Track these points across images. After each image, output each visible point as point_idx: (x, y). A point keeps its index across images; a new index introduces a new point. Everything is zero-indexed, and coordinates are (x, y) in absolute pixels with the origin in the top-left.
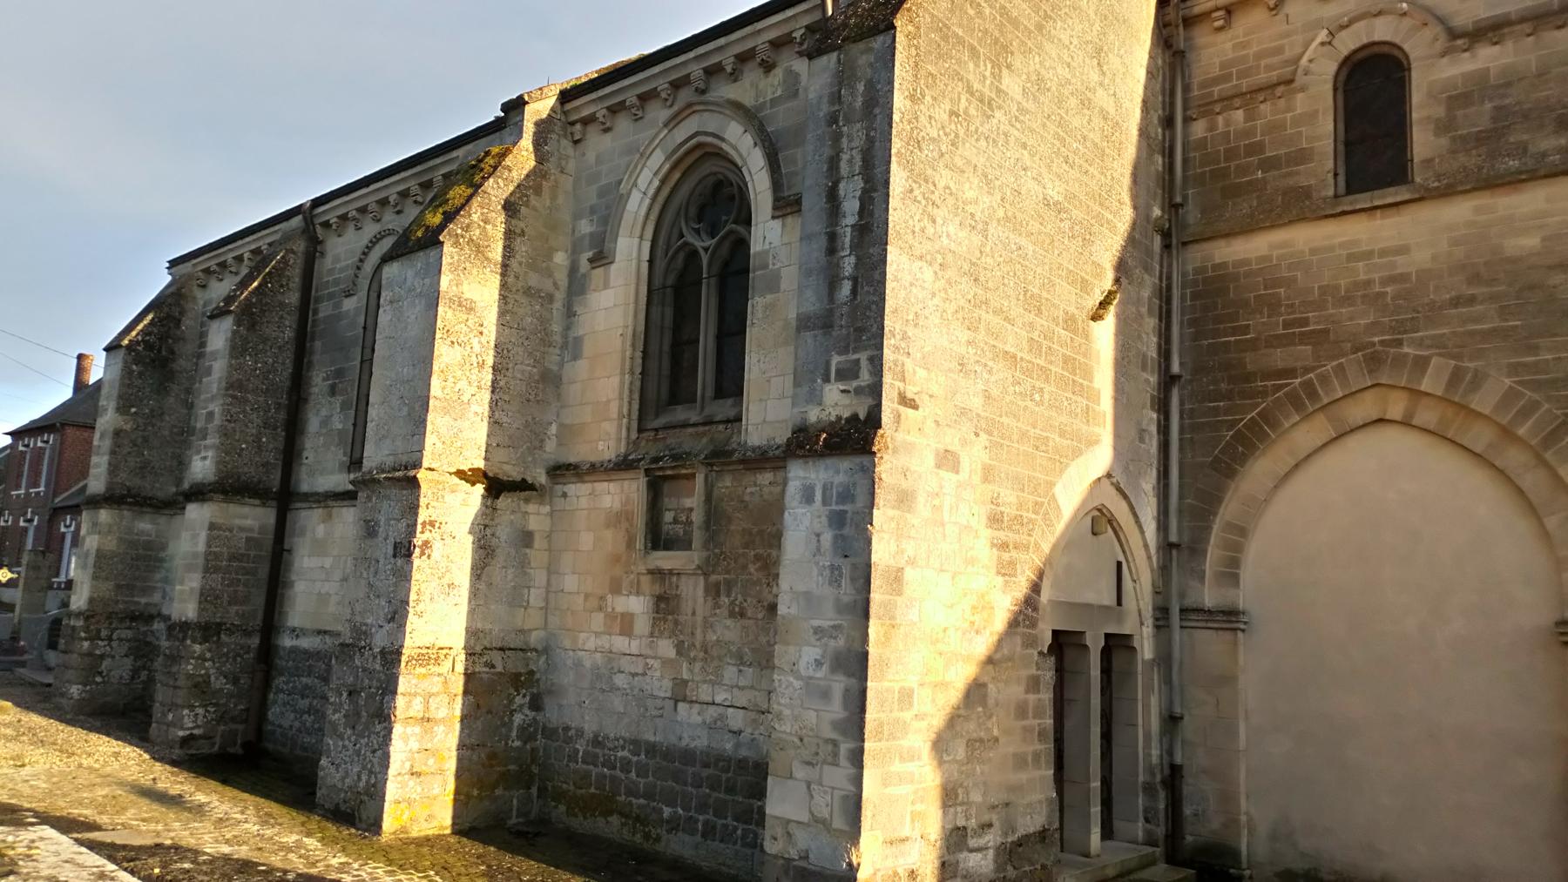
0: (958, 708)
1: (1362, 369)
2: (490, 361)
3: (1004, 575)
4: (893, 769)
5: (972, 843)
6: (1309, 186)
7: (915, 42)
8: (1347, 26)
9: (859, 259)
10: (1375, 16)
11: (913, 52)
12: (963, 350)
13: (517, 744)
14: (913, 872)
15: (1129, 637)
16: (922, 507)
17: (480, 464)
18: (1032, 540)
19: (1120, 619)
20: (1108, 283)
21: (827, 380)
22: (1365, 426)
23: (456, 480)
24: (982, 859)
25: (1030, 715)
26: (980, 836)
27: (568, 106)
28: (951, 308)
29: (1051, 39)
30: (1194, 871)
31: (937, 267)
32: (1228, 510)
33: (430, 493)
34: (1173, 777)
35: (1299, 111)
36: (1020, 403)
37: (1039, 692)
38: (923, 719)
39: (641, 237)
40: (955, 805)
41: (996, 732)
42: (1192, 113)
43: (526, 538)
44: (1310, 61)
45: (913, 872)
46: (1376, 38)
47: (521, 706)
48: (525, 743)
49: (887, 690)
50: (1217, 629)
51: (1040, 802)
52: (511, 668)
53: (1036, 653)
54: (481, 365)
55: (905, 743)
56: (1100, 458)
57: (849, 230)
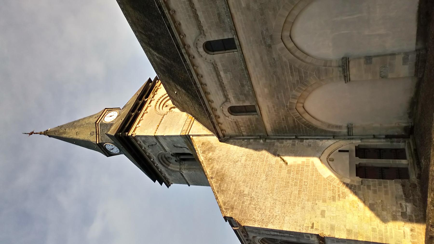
0: (375, 213)
3: (345, 197)
4: (389, 235)
5: (405, 210)
6: (256, 118)
7: (245, 220)
8: (225, 115)
9: (286, 233)
10: (223, 111)
11: (247, 221)
12: (300, 208)
14: (411, 230)
15: (356, 147)
16: (333, 223)
18: (337, 186)
19: (352, 151)
20: (279, 159)
21: (310, 239)
22: (304, 109)
24: (408, 207)
25: (376, 188)
26: (403, 207)
28: (292, 212)
29: (235, 178)
30: (411, 136)
31: (285, 215)
32: (325, 128)
34: (388, 137)
35: (241, 120)
36: (308, 189)
37: (370, 185)
38: (378, 225)
40: (396, 216)
41: (380, 201)
42: (242, 135)
44: (231, 119)
45: (411, 230)
46: (227, 111)
49: (372, 236)
50: (352, 130)
51: (395, 186)
53: (362, 186)
55: (383, 231)
56: (315, 160)
57: (280, 234)
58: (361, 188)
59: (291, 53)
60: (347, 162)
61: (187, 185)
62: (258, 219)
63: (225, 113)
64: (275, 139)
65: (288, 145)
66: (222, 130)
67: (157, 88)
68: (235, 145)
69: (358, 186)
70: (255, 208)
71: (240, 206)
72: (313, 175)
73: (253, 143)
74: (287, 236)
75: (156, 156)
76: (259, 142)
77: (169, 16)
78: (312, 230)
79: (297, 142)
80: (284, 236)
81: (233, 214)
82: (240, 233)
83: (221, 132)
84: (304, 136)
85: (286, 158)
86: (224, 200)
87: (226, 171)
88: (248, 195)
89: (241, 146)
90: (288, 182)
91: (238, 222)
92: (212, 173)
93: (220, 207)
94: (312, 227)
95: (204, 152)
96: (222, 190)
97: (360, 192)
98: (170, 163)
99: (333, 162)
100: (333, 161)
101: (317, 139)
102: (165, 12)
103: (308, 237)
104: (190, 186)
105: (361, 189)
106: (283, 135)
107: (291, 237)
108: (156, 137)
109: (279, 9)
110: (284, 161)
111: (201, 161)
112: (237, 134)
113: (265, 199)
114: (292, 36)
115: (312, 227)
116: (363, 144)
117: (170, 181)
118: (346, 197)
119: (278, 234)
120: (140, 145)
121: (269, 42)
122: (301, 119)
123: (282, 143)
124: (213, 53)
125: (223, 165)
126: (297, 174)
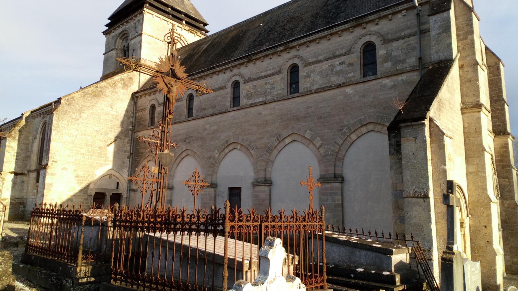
1: (412, 125)
2: (16, 155)
13: (20, 213)
15: (121, 194)
17: (13, 171)
20: (113, 140)
23: (8, 173)
27: (33, 114)
29: (96, 106)
33: (410, 154)
39: (40, 135)
42: (137, 112)
43: (23, 182)
47: (21, 207)
48: (22, 213)
52: (19, 201)
53: (87, 195)
54: (14, 156)
56: (109, 166)
58: (85, 195)
59: (180, 154)
60: (108, 187)
61: (104, 52)
62: (60, 124)
63: (152, 101)
64: (131, 138)
65: (126, 147)
66: (141, 96)
67: (195, 33)
68: (128, 106)
69: (87, 193)
70: (69, 122)
71: (70, 111)
72: (97, 163)
73: (129, 121)
74: (47, 144)
75: (128, 28)
76: (130, 125)
77: (209, 73)
78: (52, 161)
79: (128, 154)
80: (47, 142)
81: (63, 105)
82: (47, 109)
83: (139, 95)
84: (132, 159)
85: (113, 146)
86: (76, 97)
87: (103, 99)
88: (80, 117)
89: (127, 111)
90: (91, 146)
91: (57, 108)
92: (101, 87)
93: (69, 95)
94: (53, 161)
95: (122, 79)
96: (85, 96)
97: (82, 194)
98: (123, 40)
99: (108, 178)
100: (110, 178)
101: (129, 168)
102: (211, 71)
103: (46, 158)
104: (103, 55)
105: (84, 194)
106: (134, 144)
107: (47, 147)
108: (141, 34)
109: (201, 149)
110: (110, 144)
111: (114, 77)
112: (138, 108)
113: (77, 129)
114: (188, 156)
115: (53, 161)
116: (123, 198)
117: (108, 36)
118: (78, 185)
119: (48, 138)
120: (136, 16)
121: (187, 141)
122: (143, 158)
123: (127, 143)
124: (188, 99)
125: (108, 96)
126: (99, 153)
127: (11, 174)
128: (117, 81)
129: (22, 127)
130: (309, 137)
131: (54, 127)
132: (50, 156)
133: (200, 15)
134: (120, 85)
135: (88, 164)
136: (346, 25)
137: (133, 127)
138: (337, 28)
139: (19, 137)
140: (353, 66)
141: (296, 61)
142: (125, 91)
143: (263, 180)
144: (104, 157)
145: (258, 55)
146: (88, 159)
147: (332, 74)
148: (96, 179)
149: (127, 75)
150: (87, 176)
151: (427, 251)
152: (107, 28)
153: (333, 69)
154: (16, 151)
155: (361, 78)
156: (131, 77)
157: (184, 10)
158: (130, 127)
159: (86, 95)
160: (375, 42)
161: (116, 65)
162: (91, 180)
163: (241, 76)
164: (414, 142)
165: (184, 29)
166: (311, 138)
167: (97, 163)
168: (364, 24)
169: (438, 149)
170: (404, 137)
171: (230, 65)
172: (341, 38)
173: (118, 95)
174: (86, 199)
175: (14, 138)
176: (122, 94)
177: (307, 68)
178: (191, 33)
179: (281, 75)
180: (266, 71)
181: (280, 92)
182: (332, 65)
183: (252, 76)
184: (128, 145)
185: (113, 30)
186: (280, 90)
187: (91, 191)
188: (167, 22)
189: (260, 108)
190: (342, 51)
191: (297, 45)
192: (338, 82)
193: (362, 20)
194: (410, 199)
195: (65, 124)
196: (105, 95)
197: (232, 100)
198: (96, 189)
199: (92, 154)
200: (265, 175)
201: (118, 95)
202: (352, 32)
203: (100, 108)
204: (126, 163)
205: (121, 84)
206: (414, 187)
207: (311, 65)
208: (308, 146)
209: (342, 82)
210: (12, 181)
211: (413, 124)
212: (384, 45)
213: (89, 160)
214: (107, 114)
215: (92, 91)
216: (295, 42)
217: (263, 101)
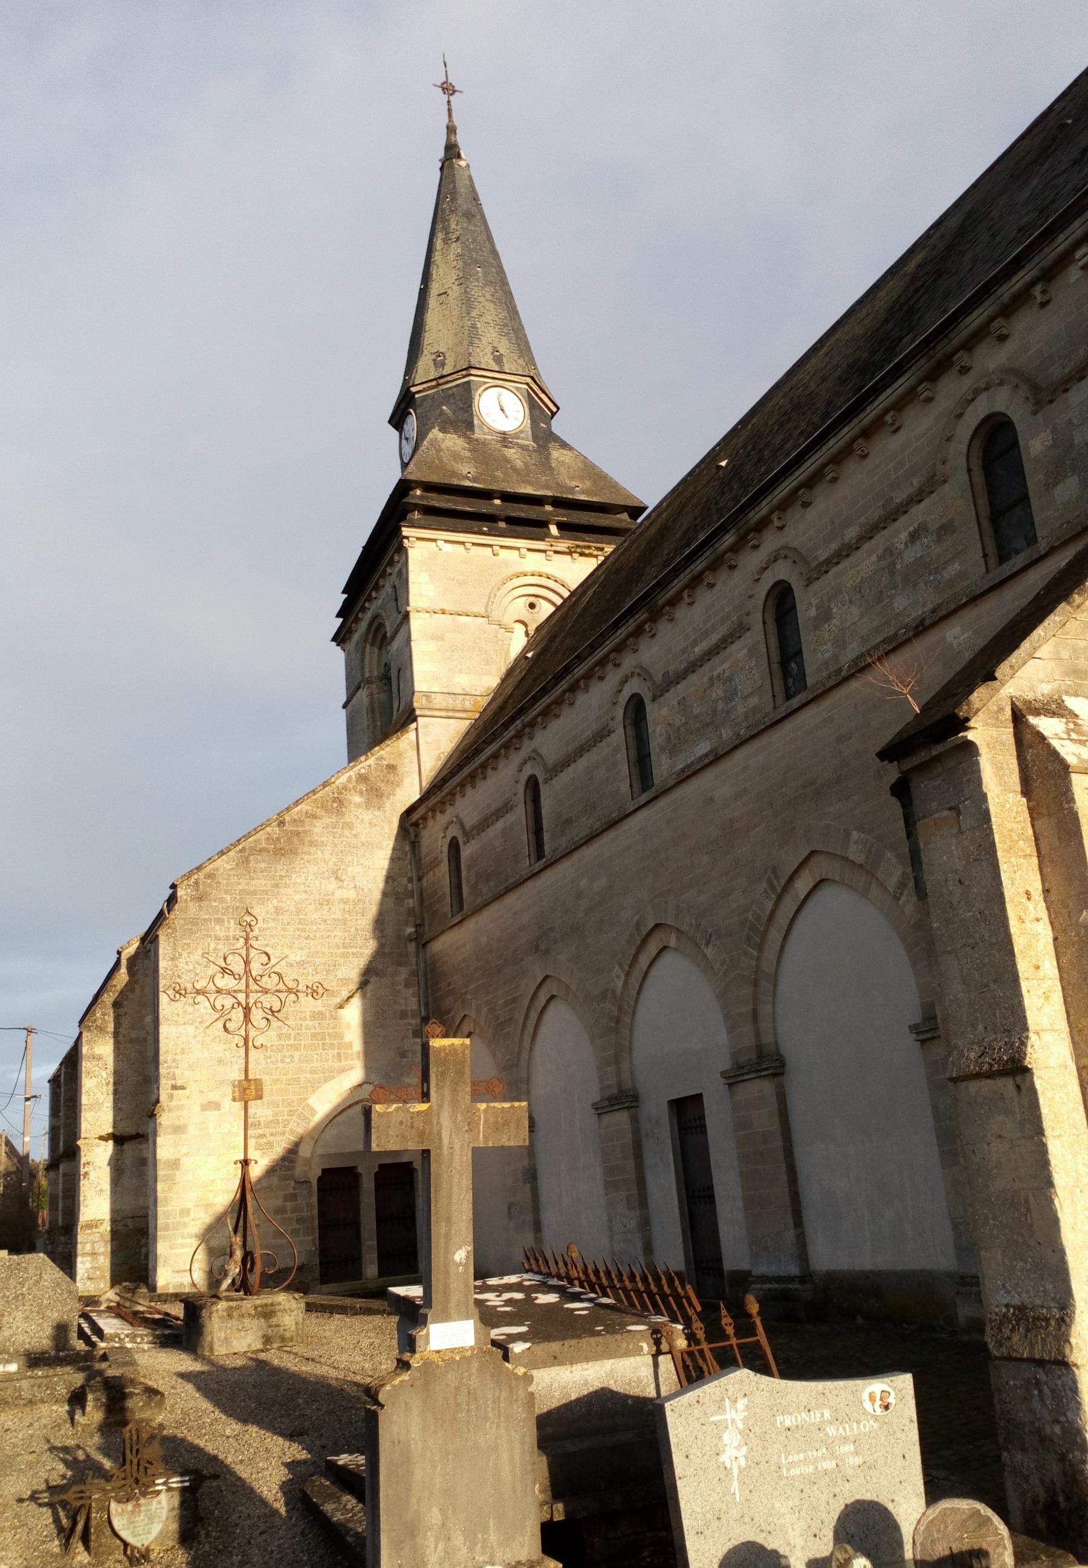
1: (937, 759)
17: (110, 1130)
20: (353, 986)
23: (97, 1141)
29: (286, 886)
53: (292, 1183)
54: (107, 1084)
61: (344, 699)
62: (181, 965)
66: (424, 818)
67: (595, 553)
69: (293, 1175)
71: (207, 917)
72: (313, 1072)
76: (406, 924)
78: (169, 1087)
86: (222, 870)
87: (306, 857)
89: (390, 878)
92: (295, 821)
93: (199, 868)
94: (174, 1087)
96: (248, 861)
97: (275, 1180)
106: (429, 984)
115: (174, 1087)
123: (407, 985)
125: (323, 844)
126: (314, 1036)
127: (103, 1143)
128: (345, 788)
129: (121, 992)
130: (860, 859)
131: (164, 978)
132: (163, 1071)
133: (614, 486)
134: (357, 799)
135: (284, 1078)
136: (901, 381)
137: (417, 926)
138: (877, 403)
139: (115, 1024)
140: (954, 532)
141: (782, 571)
142: (376, 813)
143: (754, 1056)
144: (332, 1044)
145: (670, 586)
146: (282, 1061)
147: (895, 587)
148: (318, 1124)
149: (377, 759)
150: (286, 1117)
151: (1053, 1323)
152: (341, 620)
153: (893, 564)
154: (112, 1069)
155: (988, 571)
156: (392, 762)
157: (548, 487)
158: (410, 930)
159: (252, 858)
160: (1009, 413)
161: (373, 734)
162: (300, 1130)
163: (643, 673)
164: (955, 831)
165: (556, 552)
166: (867, 858)
167: (313, 1072)
168: (958, 355)
169: (1059, 839)
170: (924, 817)
171: (608, 645)
172: (901, 437)
173: (354, 832)
174: (293, 1197)
175: (102, 1029)
176: (367, 826)
177: (816, 586)
178: (582, 558)
179: (748, 639)
180: (706, 634)
181: (753, 701)
182: (889, 551)
183: (672, 667)
184: (411, 990)
185: (353, 625)
186: (752, 693)
187: (307, 1168)
188: (489, 549)
189: (707, 780)
190: (912, 484)
191: (772, 512)
192: (916, 613)
193: (946, 341)
194: (973, 1086)
195: (197, 963)
196: (312, 843)
197: (635, 771)
198: (323, 1156)
199: (291, 1042)
200: (758, 1035)
201: (354, 832)
202: (929, 400)
203: (302, 888)
204: (410, 1055)
205: (361, 793)
206: (981, 1027)
207: (827, 572)
208: (865, 894)
209: (929, 606)
210: (109, 1164)
211: (934, 753)
212: (1040, 414)
213: (284, 1065)
214: (325, 902)
215: (268, 839)
216: (764, 503)
217: (711, 752)
